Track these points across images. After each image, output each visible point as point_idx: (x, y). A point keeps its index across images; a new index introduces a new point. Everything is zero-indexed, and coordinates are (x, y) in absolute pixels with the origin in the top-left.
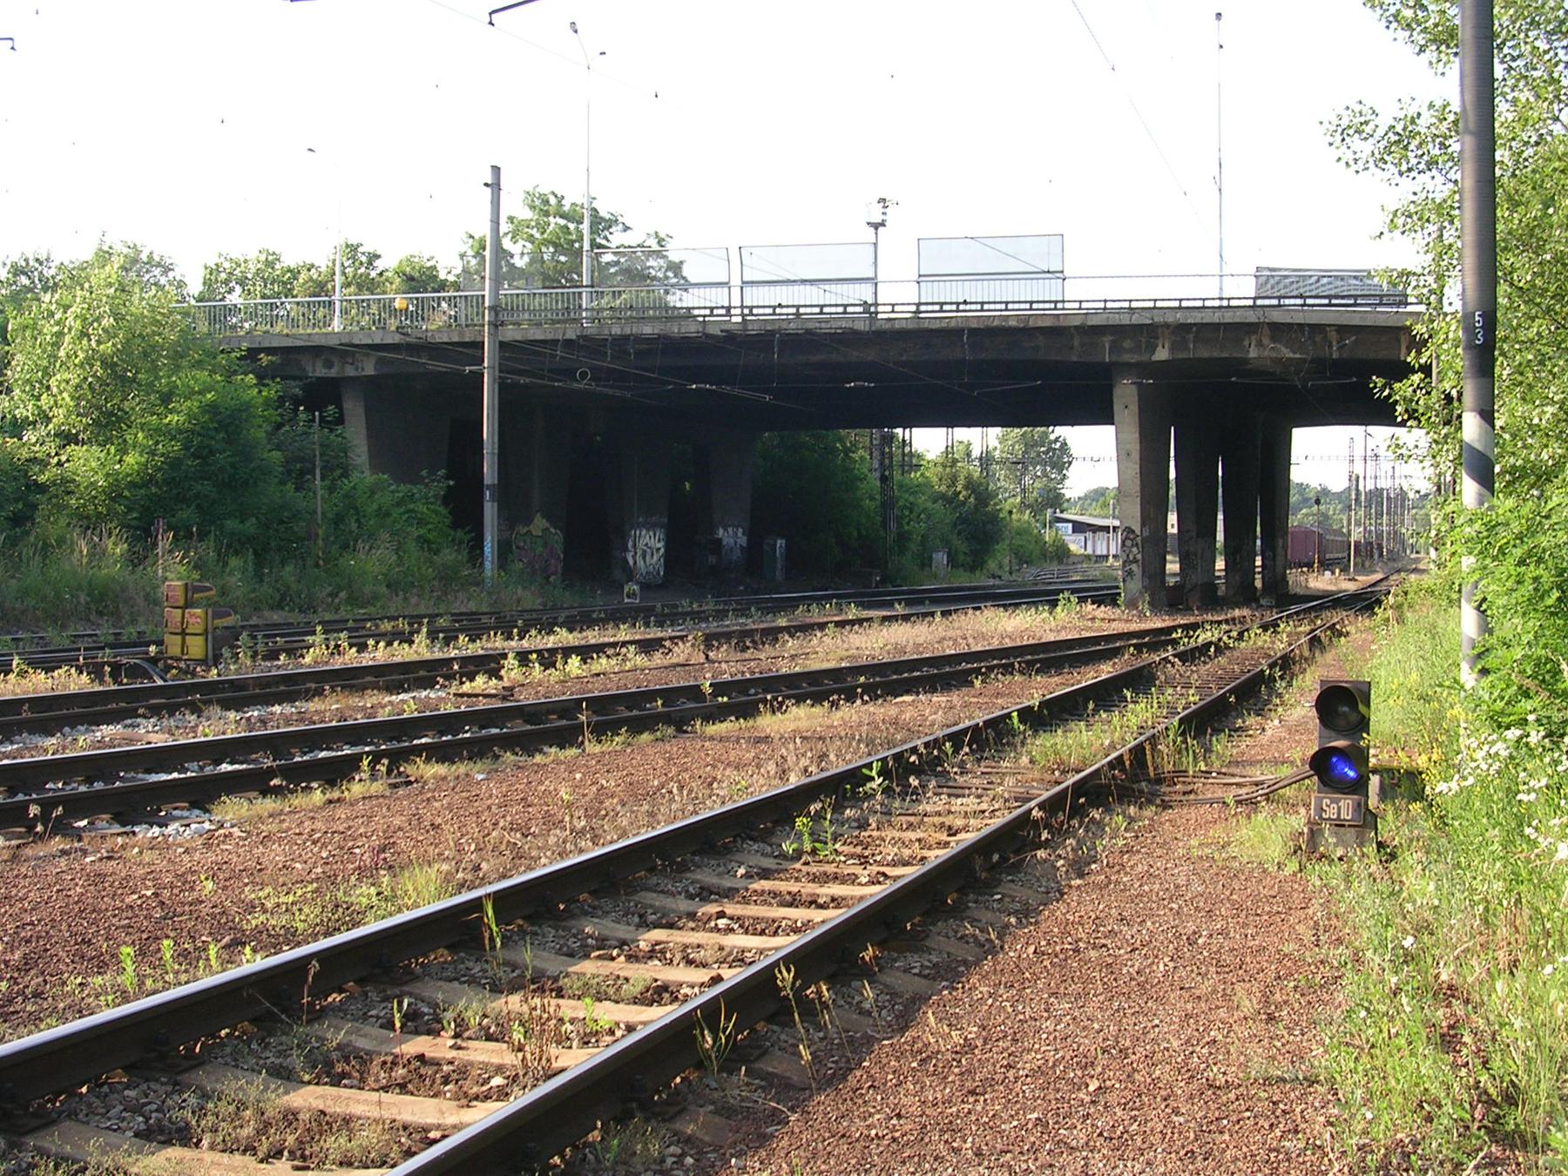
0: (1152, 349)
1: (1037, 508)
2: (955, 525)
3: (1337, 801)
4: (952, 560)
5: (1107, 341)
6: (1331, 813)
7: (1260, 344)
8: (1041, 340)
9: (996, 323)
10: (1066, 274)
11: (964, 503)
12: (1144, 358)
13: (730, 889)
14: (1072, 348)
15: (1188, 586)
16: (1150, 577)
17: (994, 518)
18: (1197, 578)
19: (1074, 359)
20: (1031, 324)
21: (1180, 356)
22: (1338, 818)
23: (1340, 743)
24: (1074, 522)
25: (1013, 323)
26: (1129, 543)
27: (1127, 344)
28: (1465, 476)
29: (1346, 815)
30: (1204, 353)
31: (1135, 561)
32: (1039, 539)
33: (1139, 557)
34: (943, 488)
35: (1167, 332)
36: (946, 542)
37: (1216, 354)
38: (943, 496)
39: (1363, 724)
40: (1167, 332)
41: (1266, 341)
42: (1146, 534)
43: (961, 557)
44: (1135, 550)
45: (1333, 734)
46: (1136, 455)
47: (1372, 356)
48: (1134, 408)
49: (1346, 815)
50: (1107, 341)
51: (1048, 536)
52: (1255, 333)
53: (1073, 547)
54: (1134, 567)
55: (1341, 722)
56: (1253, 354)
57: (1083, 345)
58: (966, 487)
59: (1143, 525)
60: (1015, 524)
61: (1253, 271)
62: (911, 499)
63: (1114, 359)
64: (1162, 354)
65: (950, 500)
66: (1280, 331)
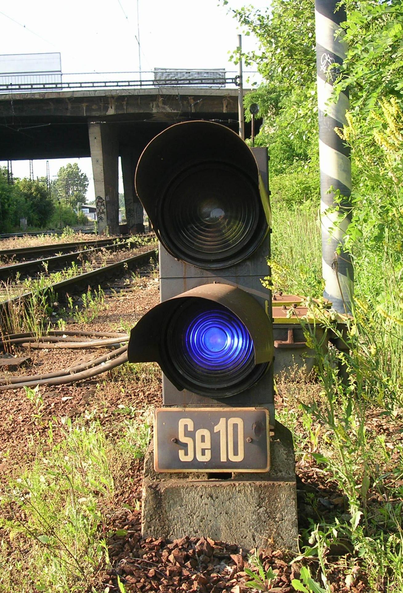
0: (106, 109)
1: (74, 204)
2: (32, 207)
3: (203, 422)
4: (30, 222)
5: (84, 105)
6: (198, 449)
7: (158, 106)
8: (52, 106)
9: (29, 97)
10: (63, 72)
11: (35, 197)
12: (103, 114)
13: (42, 347)
14: (67, 109)
15: (131, 225)
16: (111, 220)
17: (49, 204)
18: (135, 221)
19: (68, 114)
20: (46, 97)
21: (120, 112)
22: (215, 462)
23: (211, 289)
24: (90, 208)
25: (37, 97)
26: (99, 204)
27: (94, 107)
28: (316, 12)
29: (233, 452)
30: (131, 110)
31: (103, 213)
32: (74, 216)
33: (105, 210)
34: (26, 191)
35: (113, 101)
36: (27, 214)
37: (137, 111)
38: (26, 195)
39: (256, 244)
40: (113, 101)
41: (161, 105)
42: (108, 199)
43: (35, 221)
44: (103, 207)
45: (192, 270)
46: (101, 162)
47: (210, 111)
48: (99, 138)
49: (233, 452)
50: (84, 105)
51: (78, 214)
52: (155, 100)
53: (89, 219)
54: (103, 216)
55: (208, 242)
56: (154, 111)
57: (72, 108)
58: (36, 190)
59: (106, 195)
60: (64, 209)
61: (153, 70)
62: (8, 194)
63: (88, 114)
64: (111, 112)
65: (28, 196)
66: (169, 99)
